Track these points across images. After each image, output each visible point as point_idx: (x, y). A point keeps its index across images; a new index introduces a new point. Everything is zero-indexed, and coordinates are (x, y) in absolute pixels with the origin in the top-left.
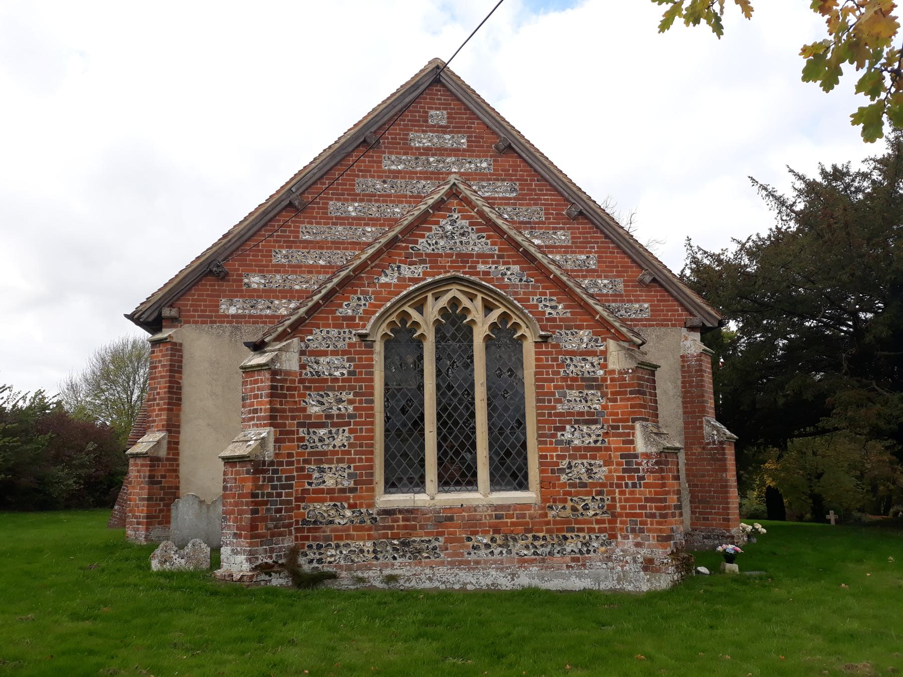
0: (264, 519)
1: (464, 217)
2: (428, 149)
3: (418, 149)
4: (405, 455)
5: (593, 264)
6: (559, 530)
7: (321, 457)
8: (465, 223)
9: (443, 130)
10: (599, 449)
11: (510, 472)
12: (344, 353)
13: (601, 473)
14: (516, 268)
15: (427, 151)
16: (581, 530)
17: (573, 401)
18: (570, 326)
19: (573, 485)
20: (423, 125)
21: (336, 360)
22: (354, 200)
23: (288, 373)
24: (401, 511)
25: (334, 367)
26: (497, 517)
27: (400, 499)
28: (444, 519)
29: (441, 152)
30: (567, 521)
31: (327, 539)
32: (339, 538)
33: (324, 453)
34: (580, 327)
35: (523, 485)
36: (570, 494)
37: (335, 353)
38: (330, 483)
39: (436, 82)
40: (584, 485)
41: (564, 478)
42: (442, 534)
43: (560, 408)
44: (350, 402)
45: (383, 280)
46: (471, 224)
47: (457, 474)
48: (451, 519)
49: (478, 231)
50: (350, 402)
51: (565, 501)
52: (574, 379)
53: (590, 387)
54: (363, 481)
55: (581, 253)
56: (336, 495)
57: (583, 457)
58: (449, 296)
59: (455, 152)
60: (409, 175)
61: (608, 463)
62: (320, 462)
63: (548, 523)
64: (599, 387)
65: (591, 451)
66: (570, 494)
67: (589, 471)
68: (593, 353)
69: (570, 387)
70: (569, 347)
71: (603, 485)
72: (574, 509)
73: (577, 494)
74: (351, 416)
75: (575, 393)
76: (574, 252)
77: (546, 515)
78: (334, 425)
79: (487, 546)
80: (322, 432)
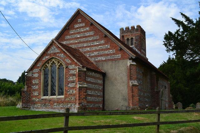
0: (24, 100)
1: (55, 46)
2: (77, 28)
3: (76, 28)
4: (46, 90)
5: (109, 47)
6: (67, 103)
7: (34, 90)
8: (55, 47)
9: (80, 23)
10: (74, 87)
11: (61, 93)
12: (38, 73)
13: (74, 92)
14: (63, 54)
15: (77, 28)
16: (71, 102)
17: (71, 79)
18: (71, 64)
19: (70, 94)
20: (77, 23)
21: (37, 74)
22: (65, 41)
23: (30, 77)
24: (44, 99)
25: (36, 75)
26: (58, 100)
27: (45, 97)
28: (50, 100)
29: (80, 27)
30: (68, 101)
31: (35, 103)
32: (36, 103)
33: (35, 90)
34: (73, 64)
35: (63, 95)
36: (69, 96)
37: (36, 73)
38: (35, 95)
39: (79, 14)
40: (71, 94)
41: (68, 93)
42: (50, 103)
43: (69, 80)
44: (38, 81)
45: (43, 59)
46: (56, 47)
47: (53, 94)
48: (51, 100)
49: (57, 48)
50: (38, 81)
51: (68, 97)
52: (71, 74)
53: (74, 76)
54: (39, 94)
55: (107, 45)
56: (36, 96)
57: (72, 89)
58: (52, 61)
59: (82, 27)
60: (74, 34)
61: (76, 90)
62: (34, 91)
63: (65, 101)
64: (75, 76)
65: (73, 88)
66: (69, 96)
67: (73, 92)
68: (74, 69)
69: (70, 76)
70: (71, 68)
71: (75, 94)
72: (70, 99)
73: (70, 96)
74: (38, 83)
75: (71, 77)
76: (105, 45)
77: (65, 100)
78: (36, 85)
79: (56, 105)
80: (35, 86)
